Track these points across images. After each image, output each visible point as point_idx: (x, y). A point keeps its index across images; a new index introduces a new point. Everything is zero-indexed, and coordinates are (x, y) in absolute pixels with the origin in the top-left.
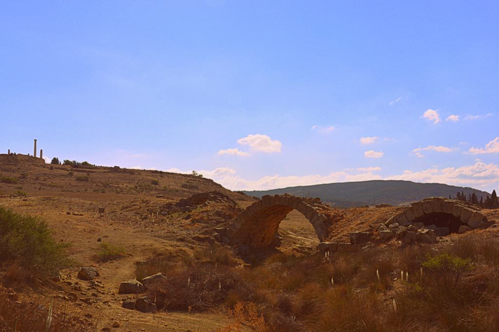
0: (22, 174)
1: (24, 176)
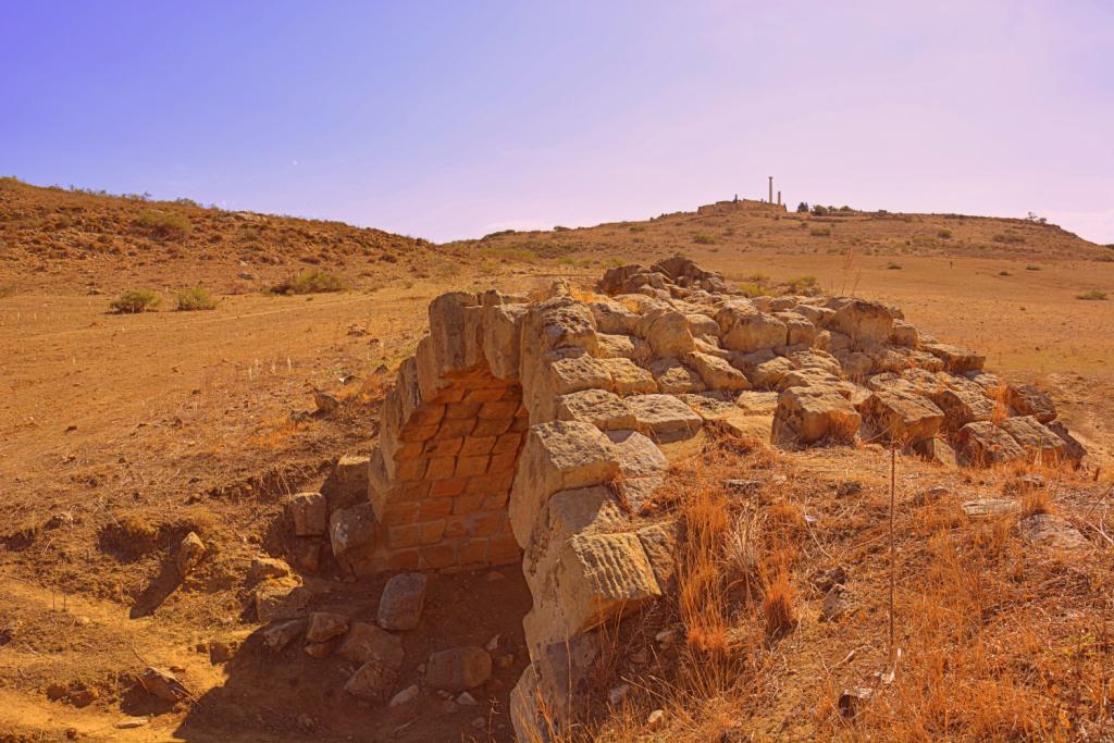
0: (728, 230)
1: (730, 233)
